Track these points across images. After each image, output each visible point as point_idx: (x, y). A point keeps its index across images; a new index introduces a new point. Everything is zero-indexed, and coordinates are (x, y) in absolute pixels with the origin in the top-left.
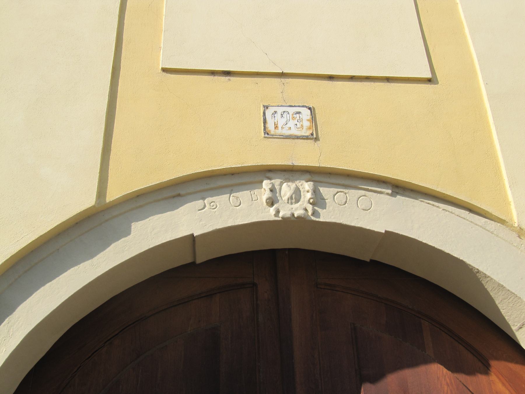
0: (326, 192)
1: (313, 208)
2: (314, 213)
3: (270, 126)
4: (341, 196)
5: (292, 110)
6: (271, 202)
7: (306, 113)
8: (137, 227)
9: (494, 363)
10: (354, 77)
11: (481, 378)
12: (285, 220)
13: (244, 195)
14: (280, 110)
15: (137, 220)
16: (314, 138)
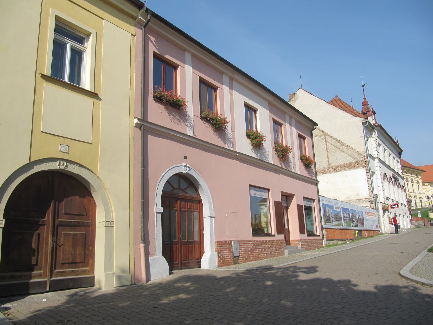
2: (66, 168)
3: (61, 149)
7: (68, 147)
8: (35, 167)
12: (61, 169)
14: (63, 146)
16: (68, 153)
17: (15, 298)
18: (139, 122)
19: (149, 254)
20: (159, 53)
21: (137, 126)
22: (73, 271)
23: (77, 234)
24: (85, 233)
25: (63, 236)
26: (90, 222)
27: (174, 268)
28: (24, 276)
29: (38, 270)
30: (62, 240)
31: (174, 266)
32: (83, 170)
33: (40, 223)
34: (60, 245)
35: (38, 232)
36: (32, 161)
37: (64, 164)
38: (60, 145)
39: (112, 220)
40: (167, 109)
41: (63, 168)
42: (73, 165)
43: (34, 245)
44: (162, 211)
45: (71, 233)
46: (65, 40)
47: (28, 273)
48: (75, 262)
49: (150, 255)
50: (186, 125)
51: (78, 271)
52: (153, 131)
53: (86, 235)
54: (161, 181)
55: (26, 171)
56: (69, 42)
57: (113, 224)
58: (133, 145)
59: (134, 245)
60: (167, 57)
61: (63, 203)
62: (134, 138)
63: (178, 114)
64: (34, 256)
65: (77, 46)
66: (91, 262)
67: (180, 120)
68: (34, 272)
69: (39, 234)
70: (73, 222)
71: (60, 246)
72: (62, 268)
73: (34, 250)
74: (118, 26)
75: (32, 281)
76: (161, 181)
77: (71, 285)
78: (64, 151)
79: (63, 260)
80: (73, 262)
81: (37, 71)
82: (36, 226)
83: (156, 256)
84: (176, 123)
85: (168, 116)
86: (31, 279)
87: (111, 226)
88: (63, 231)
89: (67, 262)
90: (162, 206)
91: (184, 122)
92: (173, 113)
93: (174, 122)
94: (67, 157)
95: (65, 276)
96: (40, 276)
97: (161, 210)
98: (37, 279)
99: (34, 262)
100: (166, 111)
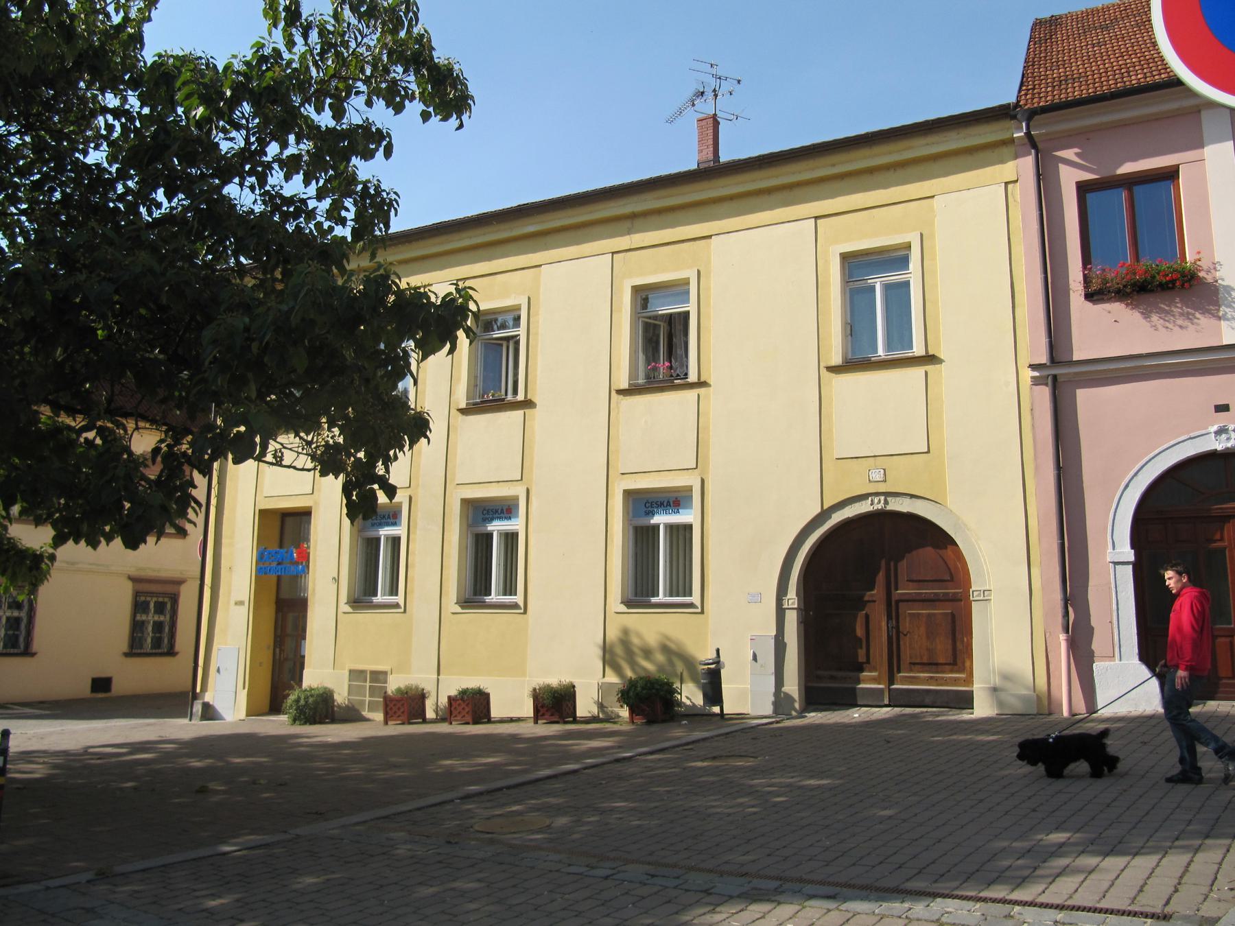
0: (889, 499)
1: (253, 458)
2: (885, 507)
3: (871, 478)
4: (893, 500)
5: (877, 471)
6: (872, 504)
7: (882, 471)
8: (833, 516)
9: (948, 546)
10: (1081, 848)
11: (945, 551)
12: (876, 510)
13: (864, 502)
14: (874, 471)
15: (833, 513)
16: (885, 481)
17: (837, 708)
18: (1036, 374)
19: (1093, 656)
20: (1097, 177)
21: (1037, 383)
22: (931, 677)
23: (934, 614)
24: (952, 613)
25: (908, 619)
26: (961, 593)
27: (1219, 695)
28: (850, 678)
29: (870, 671)
30: (906, 625)
31: (1221, 689)
32: (919, 502)
33: (866, 598)
34: (905, 633)
35: (864, 612)
36: (825, 507)
37: (880, 499)
38: (869, 471)
39: (988, 588)
40: (1134, 306)
41: (880, 508)
42: (898, 498)
43: (860, 632)
44: (1132, 558)
45: (923, 613)
46: (869, 281)
47: (851, 674)
48: (935, 662)
49: (1095, 658)
50: (1219, 318)
51: (943, 678)
52: (1090, 378)
53: (953, 615)
54: (1127, 486)
55: (822, 524)
56: (876, 283)
57: (990, 595)
58: (1030, 427)
59: (1047, 636)
60: (1127, 168)
61: (903, 564)
62: (1032, 410)
63: (1181, 300)
64: (861, 648)
65: (895, 277)
66: (967, 664)
67: (1188, 313)
68: (864, 674)
69: (867, 616)
70: (926, 593)
71: (905, 635)
72: (911, 671)
73: (860, 640)
74: (969, 189)
75: (860, 686)
76: (1127, 486)
77: (928, 701)
78: (876, 480)
79: (911, 658)
80: (931, 661)
81: (821, 364)
82: (860, 604)
83: (1117, 661)
84: (1177, 328)
85: (1143, 321)
86: (859, 684)
87: (986, 598)
88: (908, 611)
89: (918, 661)
90: (1134, 545)
91: (1210, 313)
92: (1162, 306)
93: (1167, 328)
94: (882, 488)
95: (941, 685)
96: (874, 680)
97: (1130, 555)
98: (870, 684)
99: (862, 658)
100: (1134, 311)
